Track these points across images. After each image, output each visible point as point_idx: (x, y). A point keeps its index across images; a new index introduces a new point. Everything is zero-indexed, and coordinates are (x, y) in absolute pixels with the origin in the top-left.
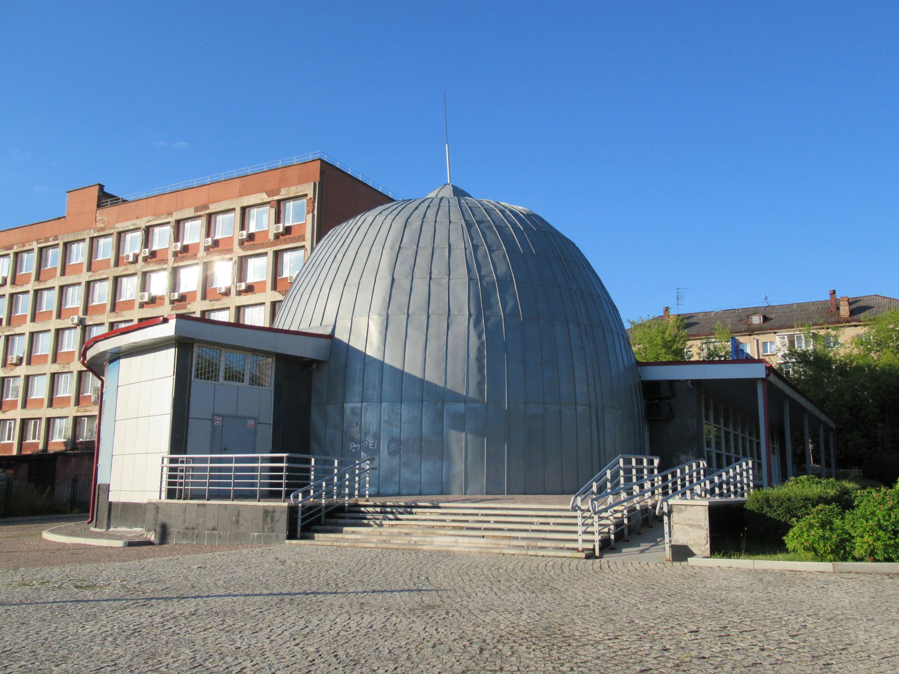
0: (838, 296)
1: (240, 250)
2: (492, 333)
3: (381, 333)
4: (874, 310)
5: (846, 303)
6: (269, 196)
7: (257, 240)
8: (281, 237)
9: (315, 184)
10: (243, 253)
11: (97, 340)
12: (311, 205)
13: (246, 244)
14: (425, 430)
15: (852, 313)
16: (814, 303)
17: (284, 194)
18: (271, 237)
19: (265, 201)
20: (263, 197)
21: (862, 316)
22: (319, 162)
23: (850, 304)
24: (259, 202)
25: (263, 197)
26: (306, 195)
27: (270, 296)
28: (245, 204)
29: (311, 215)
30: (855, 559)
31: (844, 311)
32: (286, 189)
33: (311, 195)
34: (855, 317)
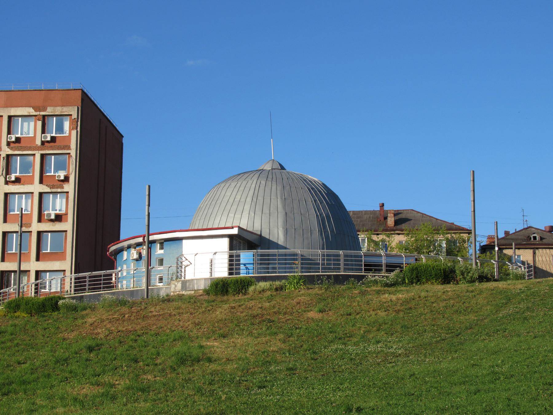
0: (386, 208)
1: (8, 150)
2: (327, 237)
3: (284, 236)
4: (412, 222)
5: (392, 215)
6: (36, 111)
7: (22, 144)
8: (46, 144)
9: (78, 108)
10: (10, 152)
11: (368, 245)
12: (75, 123)
13: (12, 145)
14: (67, 287)
15: (397, 223)
16: (366, 212)
17: (49, 111)
18: (38, 142)
19: (31, 114)
20: (31, 111)
21: (404, 226)
22: (81, 91)
23: (395, 215)
24: (26, 114)
25: (31, 111)
26: (71, 115)
27: (37, 188)
28: (12, 114)
29: (75, 131)
30: (496, 280)
31: (391, 221)
32: (52, 108)
33: (75, 116)
34: (399, 227)
